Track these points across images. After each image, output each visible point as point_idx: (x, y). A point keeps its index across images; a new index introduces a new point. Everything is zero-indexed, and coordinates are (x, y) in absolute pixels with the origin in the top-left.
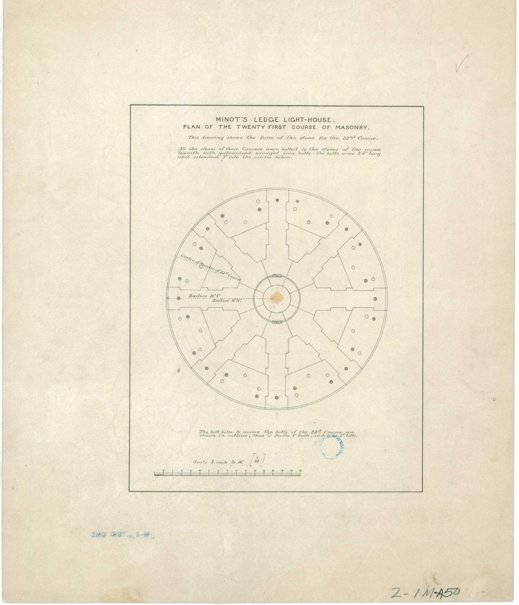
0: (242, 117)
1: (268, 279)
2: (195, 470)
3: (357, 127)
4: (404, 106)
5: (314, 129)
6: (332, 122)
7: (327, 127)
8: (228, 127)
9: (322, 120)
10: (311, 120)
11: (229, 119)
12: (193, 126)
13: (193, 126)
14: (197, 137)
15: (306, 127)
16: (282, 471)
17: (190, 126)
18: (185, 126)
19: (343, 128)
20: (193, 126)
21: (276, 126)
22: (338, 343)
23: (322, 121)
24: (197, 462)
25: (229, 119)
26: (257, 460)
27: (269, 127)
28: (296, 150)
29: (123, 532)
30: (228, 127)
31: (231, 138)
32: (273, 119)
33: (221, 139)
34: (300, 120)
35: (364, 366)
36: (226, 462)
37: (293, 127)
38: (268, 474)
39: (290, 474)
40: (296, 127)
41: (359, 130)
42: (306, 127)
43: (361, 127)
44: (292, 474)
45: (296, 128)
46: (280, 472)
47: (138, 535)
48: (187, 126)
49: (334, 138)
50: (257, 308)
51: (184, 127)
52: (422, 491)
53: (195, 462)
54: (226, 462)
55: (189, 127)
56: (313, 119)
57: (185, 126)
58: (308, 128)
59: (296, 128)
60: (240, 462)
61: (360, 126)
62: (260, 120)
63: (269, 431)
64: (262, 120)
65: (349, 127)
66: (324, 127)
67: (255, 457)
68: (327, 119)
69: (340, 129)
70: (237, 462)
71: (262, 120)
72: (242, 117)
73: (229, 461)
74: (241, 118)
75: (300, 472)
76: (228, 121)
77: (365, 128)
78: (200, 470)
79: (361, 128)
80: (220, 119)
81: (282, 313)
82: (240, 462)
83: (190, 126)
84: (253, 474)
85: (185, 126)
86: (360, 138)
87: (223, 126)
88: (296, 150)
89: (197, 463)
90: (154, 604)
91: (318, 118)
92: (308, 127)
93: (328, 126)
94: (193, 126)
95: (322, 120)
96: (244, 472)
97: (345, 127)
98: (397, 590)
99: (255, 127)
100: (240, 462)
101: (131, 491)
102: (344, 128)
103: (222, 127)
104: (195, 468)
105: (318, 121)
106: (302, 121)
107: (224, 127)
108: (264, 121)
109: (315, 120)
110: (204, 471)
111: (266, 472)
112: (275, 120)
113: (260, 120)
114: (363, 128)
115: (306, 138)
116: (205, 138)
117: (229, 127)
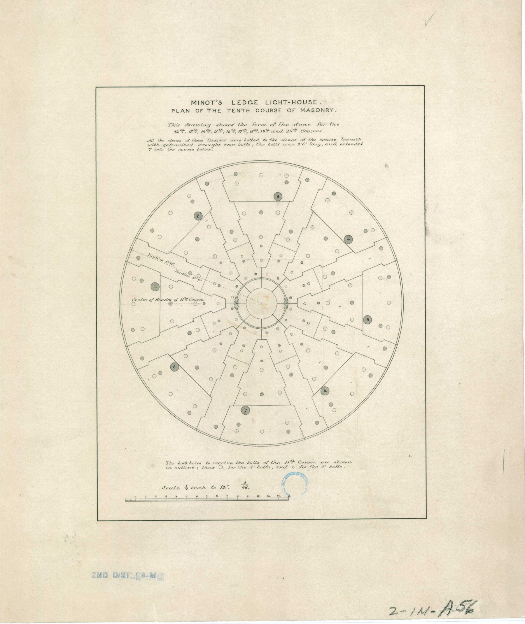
1: (244, 287)
2: (161, 496)
3: (322, 110)
4: (290, 86)
5: (218, 112)
7: (292, 110)
8: (217, 110)
9: (308, 102)
13: (308, 109)
14: (178, 125)
15: (272, 110)
17: (179, 111)
18: (173, 110)
19: (183, 112)
20: (308, 109)
21: (327, 109)
24: (166, 488)
26: (245, 486)
28: (356, 140)
29: (140, 579)
30: (217, 110)
35: (127, 349)
37: (258, 111)
42: (272, 110)
43: (327, 110)
45: (260, 111)
47: (143, 576)
50: (246, 321)
51: (172, 111)
53: (164, 488)
55: (178, 112)
57: (173, 110)
60: (223, 487)
63: (314, 466)
64: (241, 102)
66: (289, 110)
68: (278, 110)
70: (218, 487)
71: (241, 102)
72: (217, 100)
73: (208, 486)
76: (321, 109)
77: (331, 110)
80: (195, 103)
81: (306, 435)
82: (222, 487)
83: (179, 111)
85: (173, 110)
88: (356, 140)
92: (274, 110)
93: (293, 109)
94: (183, 110)
95: (308, 102)
98: (394, 609)
100: (223, 487)
102: (309, 110)
105: (303, 103)
107: (247, 110)
108: (243, 104)
112: (254, 103)
114: (330, 110)
115: (224, 125)
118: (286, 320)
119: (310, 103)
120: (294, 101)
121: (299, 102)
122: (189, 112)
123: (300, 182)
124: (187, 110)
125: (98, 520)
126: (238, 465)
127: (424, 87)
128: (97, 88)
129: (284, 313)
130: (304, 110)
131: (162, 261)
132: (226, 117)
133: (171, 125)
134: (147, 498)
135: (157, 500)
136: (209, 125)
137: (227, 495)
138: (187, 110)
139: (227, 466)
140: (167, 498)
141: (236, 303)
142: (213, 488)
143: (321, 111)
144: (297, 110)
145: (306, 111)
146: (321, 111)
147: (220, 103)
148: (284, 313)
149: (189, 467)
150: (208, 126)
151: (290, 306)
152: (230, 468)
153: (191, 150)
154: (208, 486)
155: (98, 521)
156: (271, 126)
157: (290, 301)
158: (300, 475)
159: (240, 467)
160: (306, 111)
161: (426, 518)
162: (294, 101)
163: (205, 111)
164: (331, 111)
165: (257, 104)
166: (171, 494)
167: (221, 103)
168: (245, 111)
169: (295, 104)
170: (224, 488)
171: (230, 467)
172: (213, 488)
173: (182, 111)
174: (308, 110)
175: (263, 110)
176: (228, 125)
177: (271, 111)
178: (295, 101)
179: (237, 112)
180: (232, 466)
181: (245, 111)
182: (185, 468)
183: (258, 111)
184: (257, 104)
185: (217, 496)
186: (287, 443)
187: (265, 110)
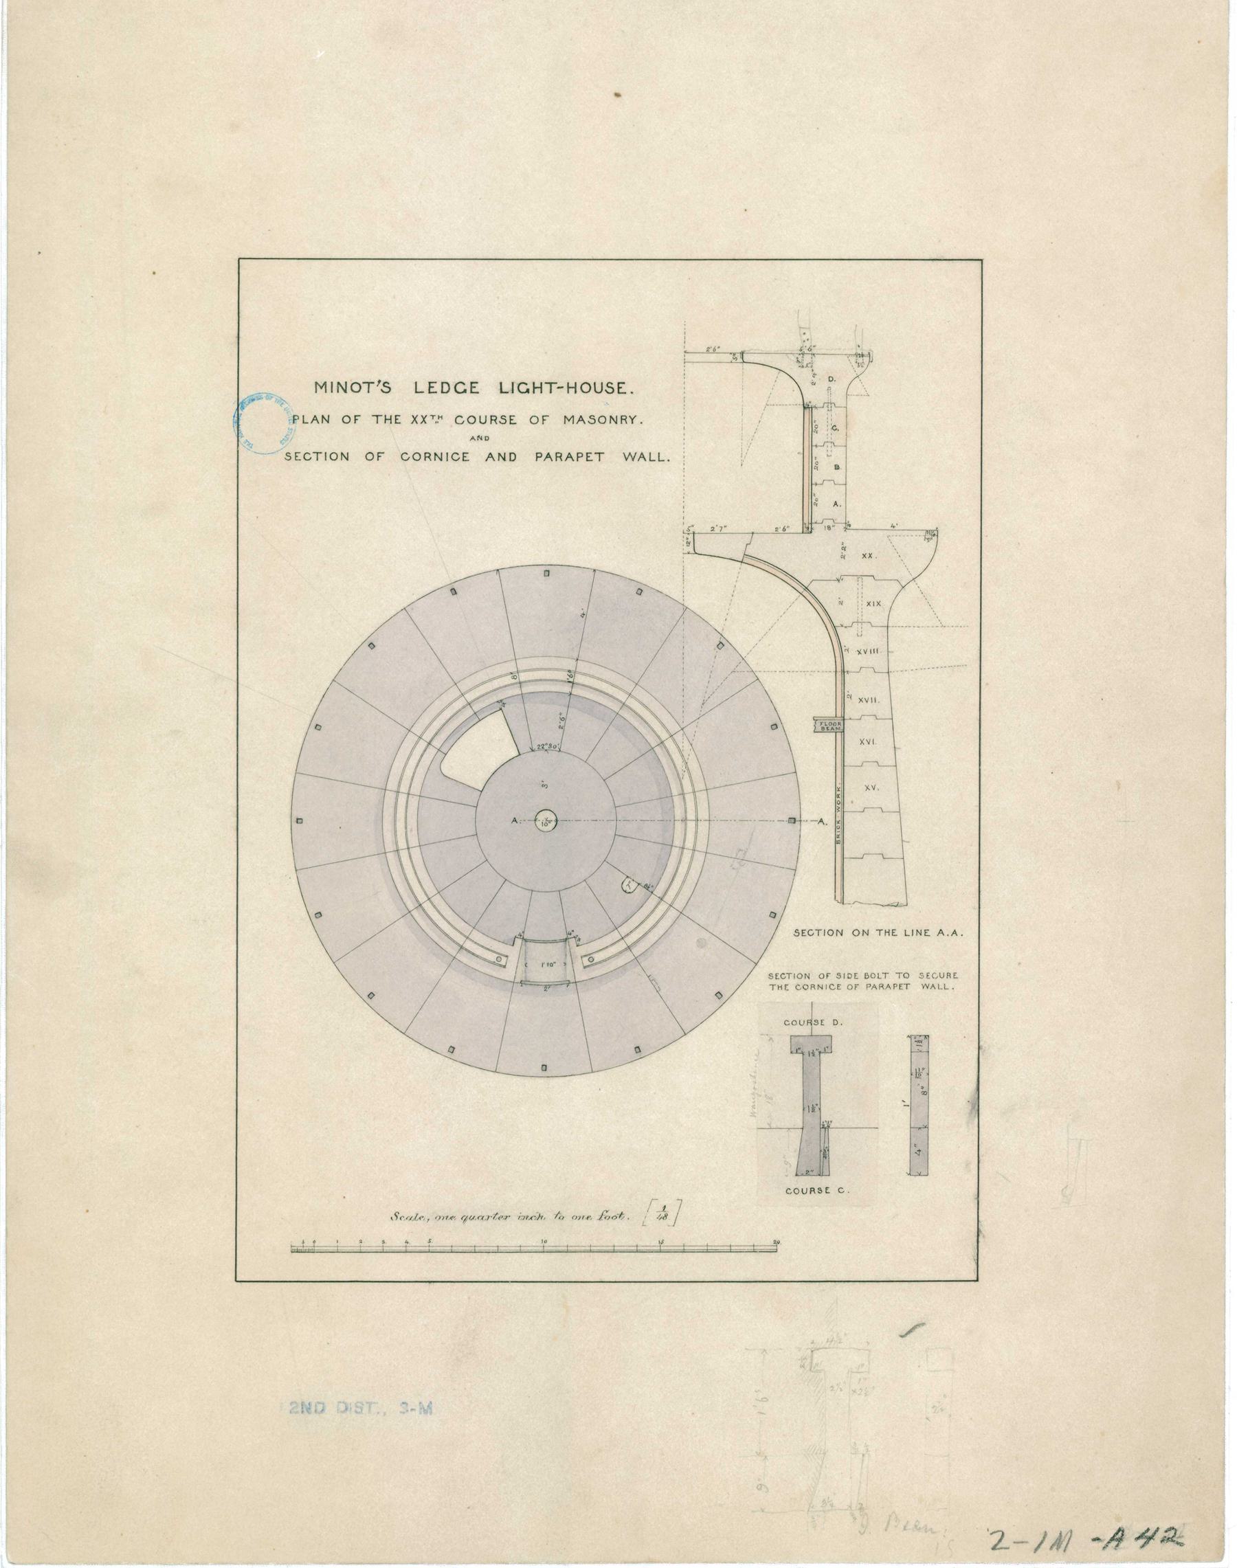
3: (440, 456)
7: (541, 419)
8: (783, 987)
9: (605, 387)
10: (536, 386)
11: (349, 386)
12: (642, 456)
16: (384, 1242)
17: (309, 419)
18: (539, 455)
23: (604, 390)
25: (349, 386)
30: (783, 987)
32: (528, 387)
36: (540, 1217)
37: (405, 457)
40: (792, 1190)
43: (623, 419)
44: (755, 1248)
45: (466, 422)
46: (401, 1245)
48: (301, 418)
51: (537, 457)
52: (238, 1280)
53: (394, 1218)
54: (540, 1217)
56: (581, 388)
57: (538, 455)
58: (628, 417)
59: (466, 422)
61: (491, 416)
64: (437, 387)
66: (856, 933)
68: (820, 1022)
71: (437, 387)
74: (376, 383)
77: (632, 420)
79: (558, 459)
80: (324, 388)
83: (309, 419)
84: (471, 1248)
85: (580, 455)
87: (383, 418)
89: (401, 1219)
90: (587, 1565)
91: (595, 383)
92: (816, 1190)
93: (543, 416)
94: (315, 418)
97: (586, 419)
99: (612, 420)
104: (397, 1234)
106: (416, 383)
107: (386, 419)
108: (442, 392)
109: (586, 388)
111: (388, 1243)
112: (469, 391)
113: (432, 390)
114: (629, 420)
117: (396, 419)
119: (610, 390)
121: (586, 388)
122: (347, 459)
123: (418, 391)
124: (504, 459)
125: (976, 1279)
127: (501, 389)
138: (504, 459)
147: (386, 390)
153: (445, 387)
158: (274, 399)
161: (416, 392)
165: (316, 392)
167: (613, 388)
168: (776, 987)
169: (534, 383)
173: (313, 420)
177: (425, 457)
178: (576, 383)
179: (348, 454)
183: (405, 457)
184: (478, 393)
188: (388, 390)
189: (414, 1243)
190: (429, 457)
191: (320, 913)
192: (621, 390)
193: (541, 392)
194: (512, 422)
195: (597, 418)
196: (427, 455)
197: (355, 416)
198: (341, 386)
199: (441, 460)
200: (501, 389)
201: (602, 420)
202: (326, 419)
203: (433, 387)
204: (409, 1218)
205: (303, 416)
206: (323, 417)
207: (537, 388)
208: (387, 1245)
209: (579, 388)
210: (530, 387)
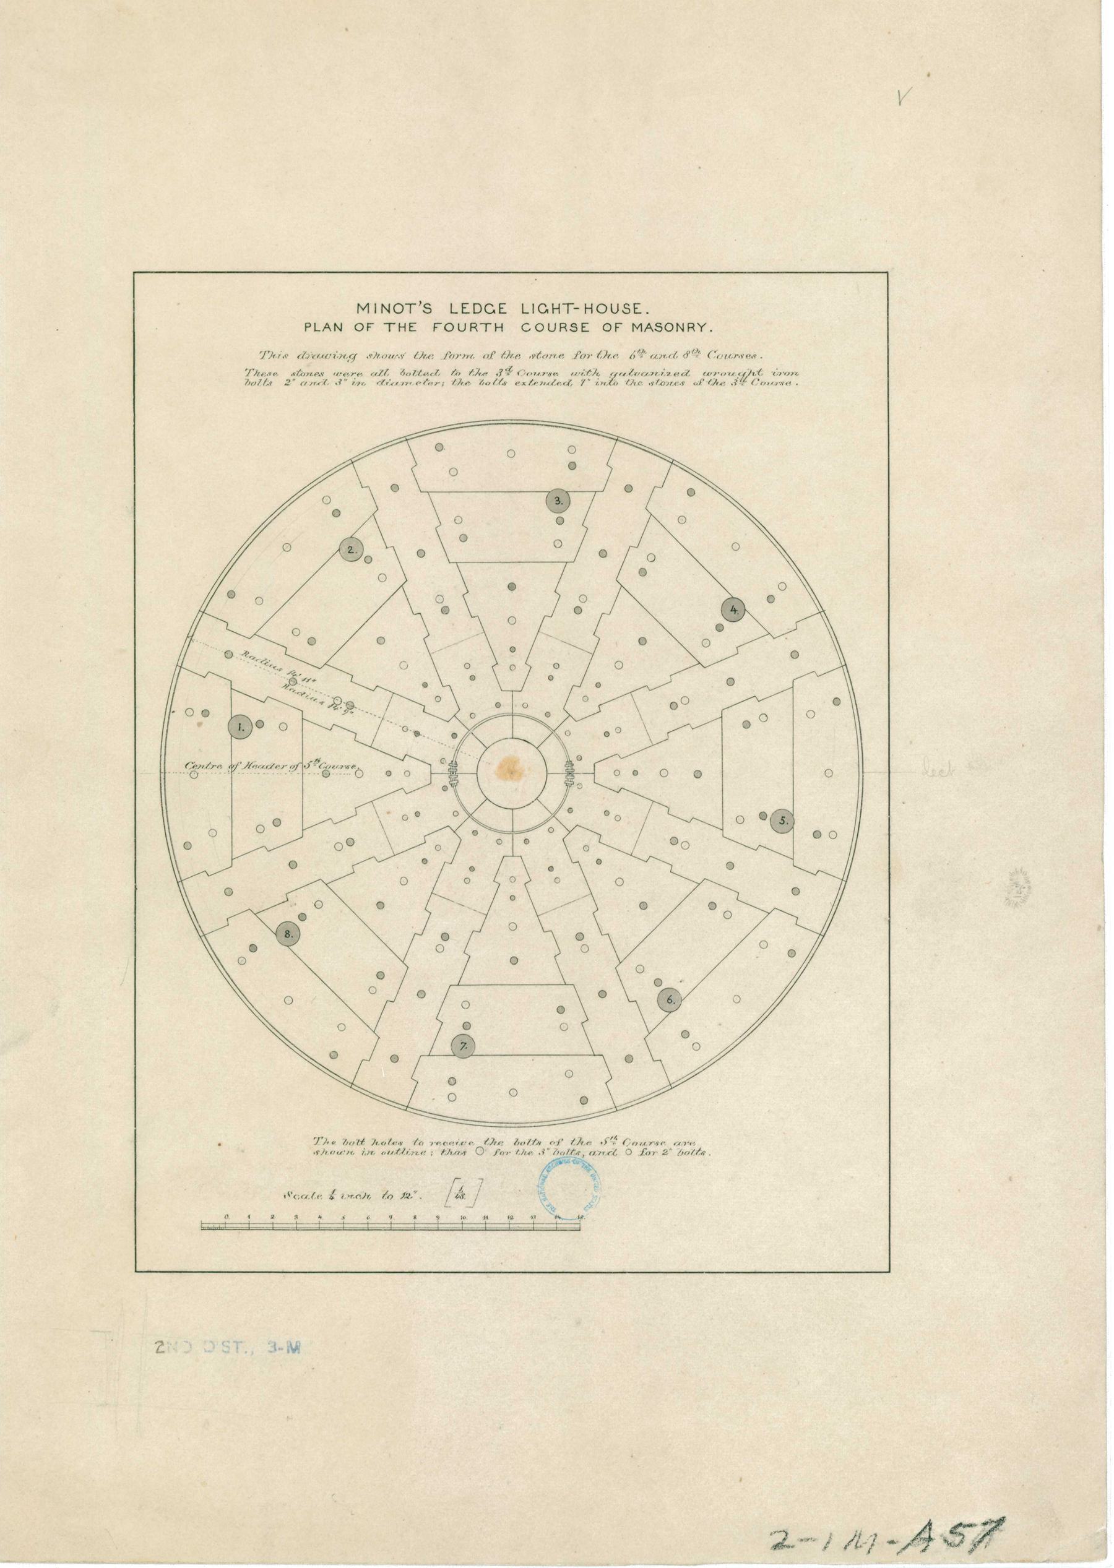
0: (421, 302)
2: (285, 1217)
6: (644, 313)
7: (366, 326)
9: (621, 308)
13: (649, 324)
14: (283, 355)
17: (320, 327)
19: (328, 329)
20: (649, 324)
21: (473, 325)
22: (328, 885)
27: (435, 327)
31: (377, 355)
33: (351, 360)
34: (564, 308)
37: (526, 327)
38: (520, 1226)
39: (271, 1226)
41: (689, 335)
43: (691, 326)
45: (533, 329)
49: (423, 356)
51: (306, 327)
52: (886, 274)
54: (332, 1198)
59: (680, 842)
62: (501, 312)
64: (469, 308)
65: (663, 326)
67: (457, 1186)
69: (643, 330)
70: (398, 1195)
71: (469, 308)
72: (421, 302)
75: (578, 1221)
77: (701, 327)
78: (320, 1217)
80: (366, 309)
83: (320, 327)
86: (712, 355)
90: (261, 1566)
92: (569, 327)
94: (327, 326)
95: (621, 308)
96: (479, 1219)
100: (406, 1196)
101: (138, 1272)
102: (329, 327)
103: (394, 328)
107: (400, 327)
108: (474, 313)
109: (398, 308)
110: (309, 1218)
111: (325, 1219)
112: (497, 311)
113: (465, 310)
114: (697, 328)
116: (306, 356)
117: (410, 327)
118: (570, 810)
119: (627, 311)
120: (589, 306)
122: (341, 330)
125: (888, 1270)
126: (516, 1148)
128: (136, 274)
129: (566, 796)
130: (640, 328)
131: (277, 672)
132: (424, 338)
133: (268, 355)
134: (417, 1221)
135: (346, 1226)
136: (352, 357)
137: (391, 1217)
139: (639, 1149)
140: (346, 1221)
141: (453, 770)
142: (387, 1196)
143: (389, 305)
144: (626, 327)
145: (644, 328)
146: (677, 331)
148: (566, 796)
149: (602, 1151)
150: (350, 357)
151: (578, 779)
152: (644, 1153)
154: (376, 1191)
155: (889, 1272)
156: (486, 360)
157: (578, 766)
159: (521, 1152)
160: (644, 328)
161: (889, 1272)
162: (589, 306)
163: (379, 329)
164: (701, 331)
165: (382, 312)
166: (309, 1212)
167: (661, 327)
168: (491, 328)
170: (407, 1197)
171: (643, 1152)
172: (387, 1196)
173: (325, 327)
174: (649, 326)
175: (449, 328)
176: (622, 374)
180: (501, 1150)
181: (491, 328)
182: (405, 1152)
183: (526, 327)
184: (382, 312)
185: (296, 1216)
186: (367, 1093)
187: (609, 309)
188: (426, 306)
189: (352, 1219)
190: (475, 327)
191: (552, 867)
192: (637, 311)
193: (592, 313)
194: (584, 329)
195: (663, 326)
196: (563, 325)
197: (368, 324)
198: (386, 309)
199: (383, 305)
200: (888, 276)
201: (669, 327)
202: (339, 328)
203: (465, 308)
204: (304, 1197)
205: (315, 324)
206: (335, 324)
207: (691, 326)
208: (324, 1222)
209: (596, 310)
210: (550, 308)
